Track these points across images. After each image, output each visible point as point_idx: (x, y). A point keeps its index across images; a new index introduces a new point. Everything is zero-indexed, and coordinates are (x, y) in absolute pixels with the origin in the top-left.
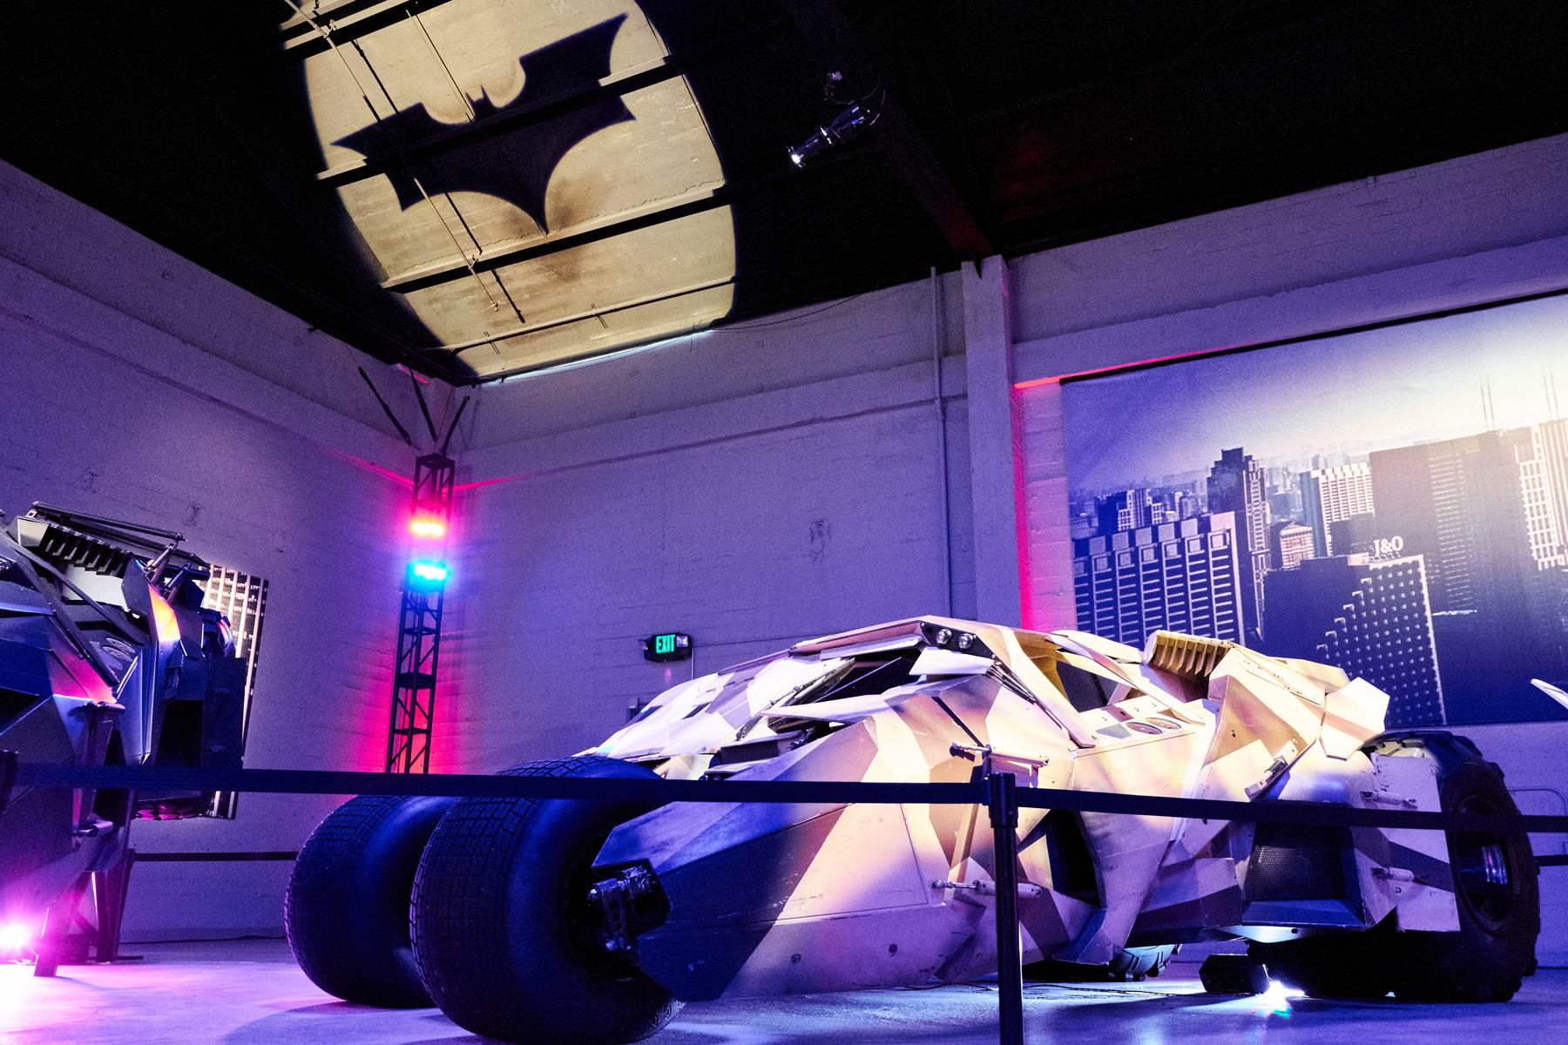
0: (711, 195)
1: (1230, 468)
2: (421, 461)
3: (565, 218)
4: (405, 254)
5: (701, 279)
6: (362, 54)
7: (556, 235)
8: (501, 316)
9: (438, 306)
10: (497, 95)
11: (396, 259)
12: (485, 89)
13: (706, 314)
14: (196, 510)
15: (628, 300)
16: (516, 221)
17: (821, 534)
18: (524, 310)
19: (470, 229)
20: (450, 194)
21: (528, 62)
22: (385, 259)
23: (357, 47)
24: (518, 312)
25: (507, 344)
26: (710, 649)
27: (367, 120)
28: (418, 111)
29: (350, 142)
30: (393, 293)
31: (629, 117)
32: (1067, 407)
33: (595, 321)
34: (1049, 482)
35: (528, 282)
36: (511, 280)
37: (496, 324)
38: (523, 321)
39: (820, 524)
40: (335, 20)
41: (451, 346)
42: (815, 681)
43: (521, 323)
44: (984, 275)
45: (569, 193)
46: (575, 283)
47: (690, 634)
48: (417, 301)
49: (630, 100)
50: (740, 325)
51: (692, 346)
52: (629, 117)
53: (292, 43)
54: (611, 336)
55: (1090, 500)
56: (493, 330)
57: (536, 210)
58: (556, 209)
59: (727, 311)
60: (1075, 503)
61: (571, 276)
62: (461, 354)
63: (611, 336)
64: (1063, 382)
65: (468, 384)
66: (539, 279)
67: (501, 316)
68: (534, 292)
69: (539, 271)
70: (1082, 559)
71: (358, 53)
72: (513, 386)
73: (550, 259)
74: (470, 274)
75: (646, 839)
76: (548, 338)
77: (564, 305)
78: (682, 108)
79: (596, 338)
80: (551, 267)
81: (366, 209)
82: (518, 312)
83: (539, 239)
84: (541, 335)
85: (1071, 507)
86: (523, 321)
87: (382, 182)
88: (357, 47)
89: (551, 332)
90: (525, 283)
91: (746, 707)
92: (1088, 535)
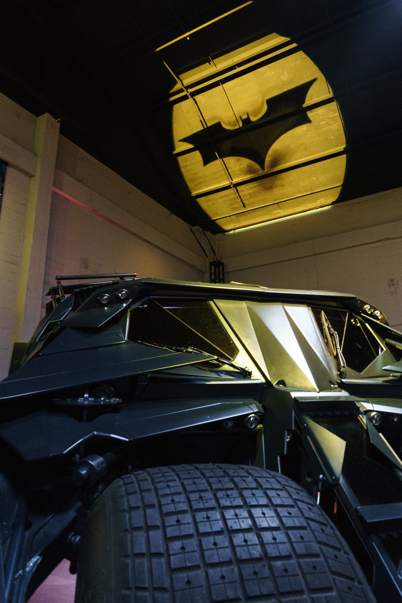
0: (343, 150)
1: (53, 288)
2: (211, 264)
8: (236, 206)
9: (210, 203)
12: (249, 114)
15: (288, 198)
17: (394, 285)
18: (246, 202)
19: (229, 171)
21: (269, 102)
22: (190, 185)
23: (194, 100)
24: (243, 204)
27: (199, 128)
28: (218, 125)
29: (185, 140)
31: (309, 121)
33: (276, 205)
36: (243, 191)
37: (233, 209)
38: (245, 207)
39: (392, 281)
40: (190, 89)
42: (322, 347)
48: (199, 200)
49: (310, 114)
51: (322, 213)
52: (309, 121)
57: (261, 163)
59: (336, 198)
61: (270, 188)
65: (220, 233)
66: (255, 190)
67: (236, 206)
74: (231, 188)
75: (235, 412)
79: (275, 212)
81: (186, 166)
82: (243, 204)
86: (245, 207)
88: (194, 100)
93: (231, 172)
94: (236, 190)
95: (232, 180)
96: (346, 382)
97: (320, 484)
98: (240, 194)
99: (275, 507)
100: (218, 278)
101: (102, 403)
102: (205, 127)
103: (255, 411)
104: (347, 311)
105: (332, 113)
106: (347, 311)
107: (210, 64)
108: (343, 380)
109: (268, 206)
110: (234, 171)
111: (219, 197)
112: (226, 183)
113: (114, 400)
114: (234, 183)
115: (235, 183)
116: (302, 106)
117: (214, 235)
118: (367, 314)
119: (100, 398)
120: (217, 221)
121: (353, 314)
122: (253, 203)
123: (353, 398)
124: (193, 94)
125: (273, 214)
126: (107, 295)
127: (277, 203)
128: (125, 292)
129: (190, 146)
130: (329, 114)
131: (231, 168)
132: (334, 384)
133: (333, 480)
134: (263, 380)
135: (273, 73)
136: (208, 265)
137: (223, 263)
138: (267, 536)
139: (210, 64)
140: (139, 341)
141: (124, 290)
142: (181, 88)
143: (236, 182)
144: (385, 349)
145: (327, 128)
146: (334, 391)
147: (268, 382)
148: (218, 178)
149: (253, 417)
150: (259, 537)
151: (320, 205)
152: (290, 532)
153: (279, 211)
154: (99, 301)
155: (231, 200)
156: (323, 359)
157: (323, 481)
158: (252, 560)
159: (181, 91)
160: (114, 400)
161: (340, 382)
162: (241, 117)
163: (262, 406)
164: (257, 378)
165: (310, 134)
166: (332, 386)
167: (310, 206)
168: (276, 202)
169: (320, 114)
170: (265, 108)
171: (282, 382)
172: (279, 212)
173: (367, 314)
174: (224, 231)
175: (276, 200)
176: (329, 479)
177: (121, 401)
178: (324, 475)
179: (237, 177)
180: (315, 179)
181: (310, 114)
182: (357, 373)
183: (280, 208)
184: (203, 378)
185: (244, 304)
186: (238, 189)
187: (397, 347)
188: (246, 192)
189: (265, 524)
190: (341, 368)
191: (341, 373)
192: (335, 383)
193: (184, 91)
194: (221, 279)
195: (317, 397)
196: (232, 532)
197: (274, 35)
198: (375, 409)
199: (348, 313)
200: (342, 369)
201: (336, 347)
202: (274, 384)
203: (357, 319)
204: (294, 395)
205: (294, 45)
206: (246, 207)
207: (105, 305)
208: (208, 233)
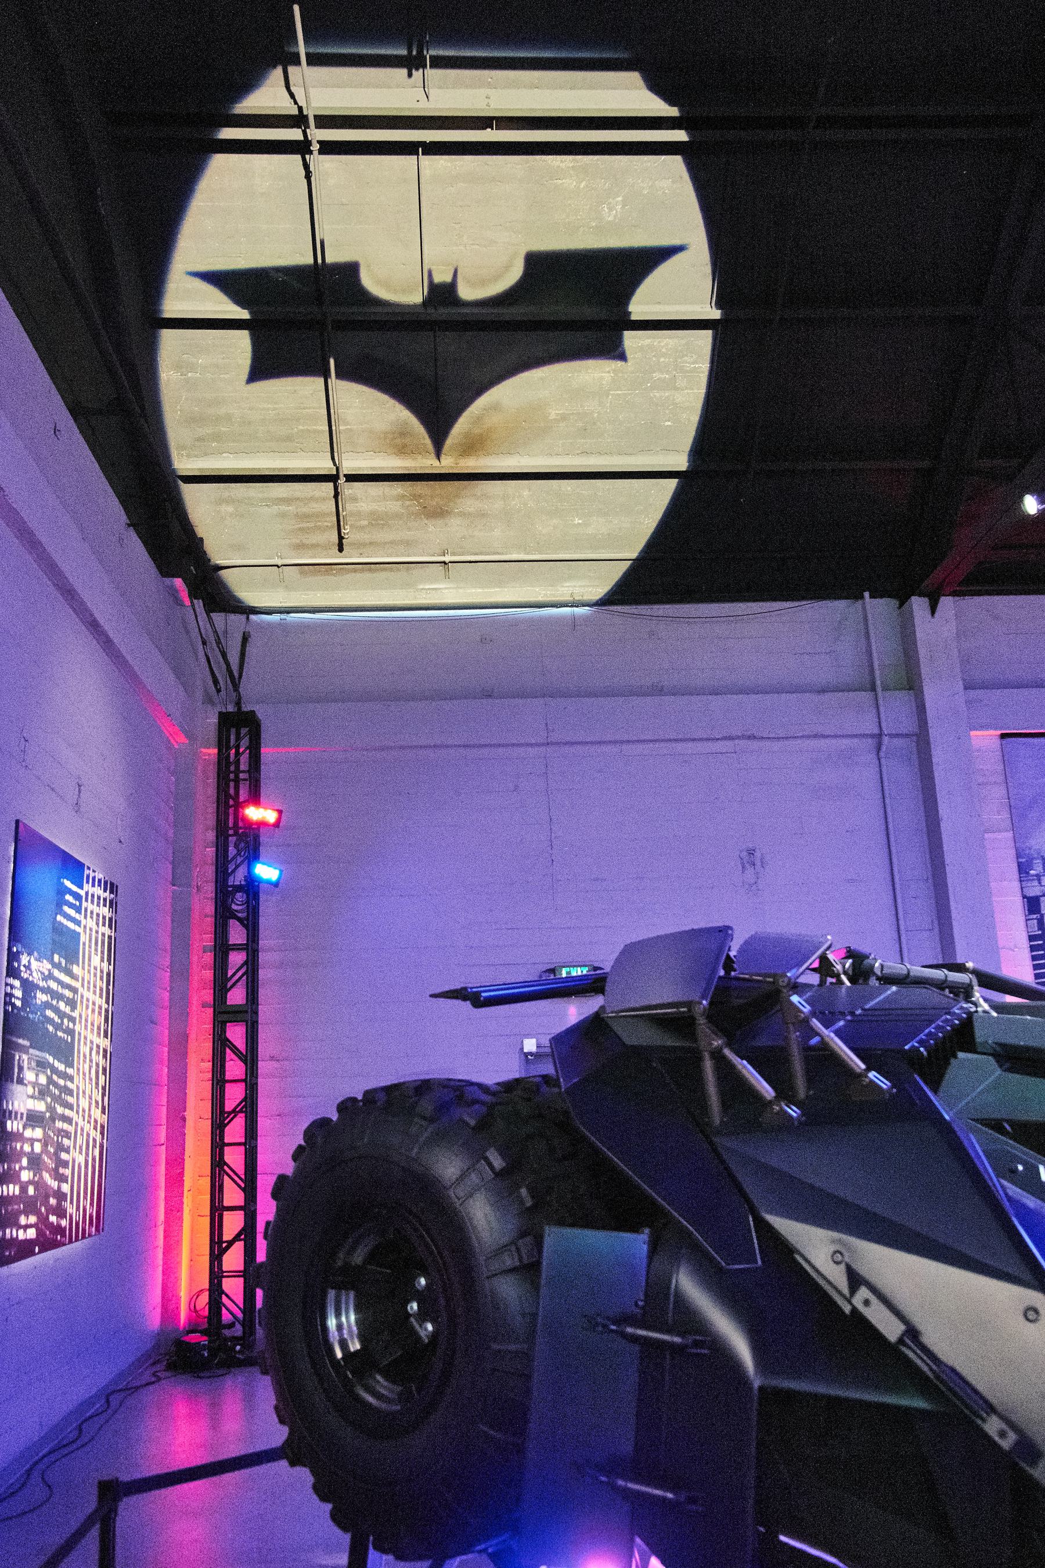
3: (472, 446)
4: (217, 437)
6: (308, 176)
7: (448, 463)
10: (472, 284)
13: (580, 586)
20: (672, 484)
23: (306, 166)
24: (341, 538)
25: (301, 573)
29: (220, 280)
30: (180, 482)
31: (622, 357)
32: (1005, 760)
33: (440, 567)
34: (996, 835)
36: (355, 499)
37: (300, 547)
38: (341, 549)
39: (751, 852)
44: (936, 615)
45: (494, 420)
46: (440, 522)
48: (189, 492)
49: (631, 339)
50: (626, 609)
52: (622, 357)
54: (446, 588)
55: (1038, 858)
58: (467, 435)
60: (1024, 860)
61: (439, 513)
62: (222, 573)
64: (1003, 736)
66: (395, 507)
68: (378, 520)
69: (402, 497)
70: (1035, 916)
71: (303, 173)
73: (420, 487)
77: (408, 543)
80: (416, 497)
82: (341, 538)
83: (428, 463)
84: (355, 571)
85: (1019, 865)
86: (341, 549)
88: (306, 166)
89: (370, 570)
90: (370, 508)
92: (1039, 894)
100: (233, 780)
105: (695, 357)
107: (410, 75)
109: (424, 565)
110: (351, 430)
120: (223, 573)
130: (686, 358)
135: (582, 185)
139: (410, 75)
140: (259, 1293)
145: (667, 394)
148: (289, 438)
153: (441, 586)
165: (617, 394)
168: (447, 559)
169: (664, 350)
170: (515, 273)
180: (579, 524)
181: (631, 339)
183: (447, 577)
188: (364, 506)
197: (634, 77)
205: (680, 136)
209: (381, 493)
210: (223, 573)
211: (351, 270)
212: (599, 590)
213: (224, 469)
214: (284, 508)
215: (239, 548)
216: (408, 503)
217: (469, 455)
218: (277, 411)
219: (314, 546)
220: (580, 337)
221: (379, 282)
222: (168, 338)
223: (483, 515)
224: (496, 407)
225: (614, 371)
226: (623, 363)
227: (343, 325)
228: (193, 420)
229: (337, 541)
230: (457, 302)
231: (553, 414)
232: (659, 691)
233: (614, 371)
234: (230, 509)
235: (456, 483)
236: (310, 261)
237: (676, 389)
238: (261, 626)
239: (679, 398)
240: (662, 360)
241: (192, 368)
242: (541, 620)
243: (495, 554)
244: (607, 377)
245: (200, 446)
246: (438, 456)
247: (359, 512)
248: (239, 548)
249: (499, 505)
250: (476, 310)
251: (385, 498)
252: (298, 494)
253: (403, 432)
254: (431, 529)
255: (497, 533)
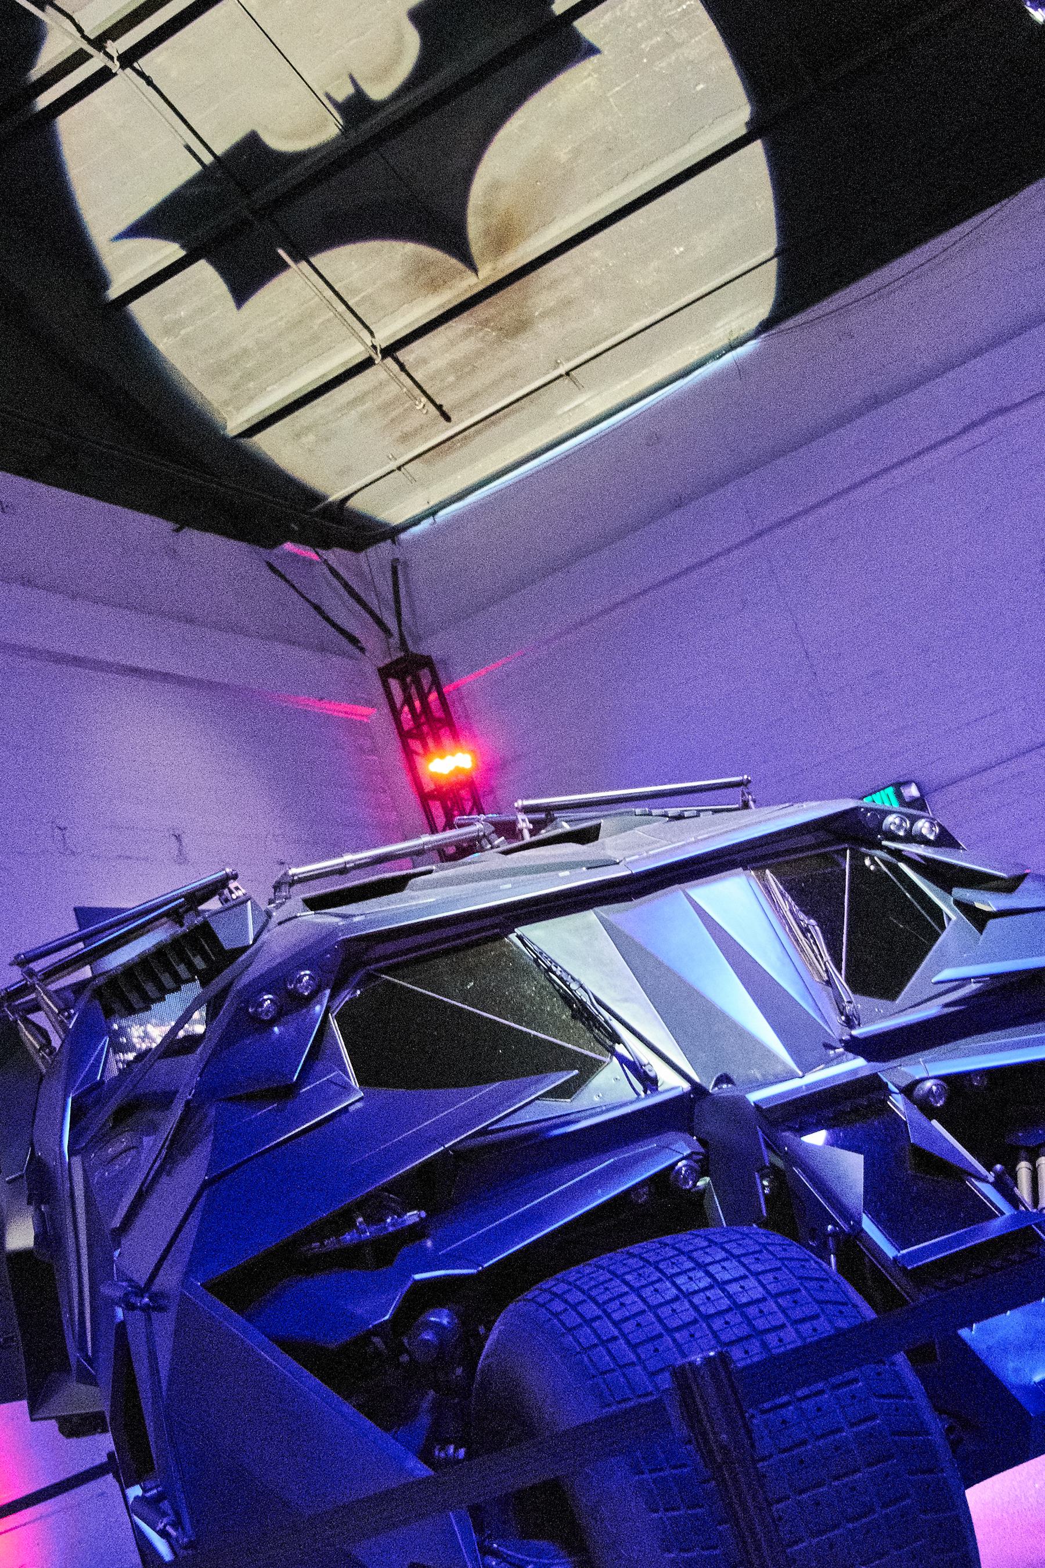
2: (385, 673)
4: (249, 376)
5: (722, 268)
6: (149, 82)
7: (489, 272)
11: (236, 387)
12: (355, 76)
14: (178, 838)
16: (420, 268)
19: (350, 303)
20: (313, 260)
23: (141, 74)
24: (439, 407)
26: (954, 791)
29: (143, 228)
30: (243, 441)
31: (592, 50)
33: (566, 381)
35: (448, 357)
36: (425, 361)
37: (405, 438)
38: (448, 419)
40: (114, 40)
41: (336, 496)
43: (446, 423)
45: (505, 200)
46: (528, 334)
47: (921, 778)
48: (266, 443)
52: (592, 50)
53: (44, 100)
54: (588, 399)
56: (402, 448)
58: (487, 232)
61: (521, 326)
63: (588, 399)
68: (464, 369)
72: (457, 523)
73: (482, 311)
76: (494, 432)
77: (513, 374)
78: (673, 13)
79: (566, 408)
80: (485, 323)
82: (439, 407)
83: (468, 284)
86: (448, 419)
87: (203, 271)
88: (141, 74)
91: (181, 1000)
93: (357, 304)
94: (395, 368)
95: (372, 333)
96: (860, 1034)
97: (831, 1242)
98: (418, 377)
99: (737, 1258)
101: (391, 1229)
102: (208, 159)
103: (685, 1154)
104: (846, 845)
106: (846, 845)
108: (854, 1032)
111: (339, 410)
112: (354, 352)
113: (412, 1216)
114: (384, 346)
115: (388, 343)
116: (552, 12)
117: (363, 554)
118: (894, 838)
119: (384, 1221)
120: (351, 503)
121: (863, 850)
122: (476, 395)
123: (877, 1067)
124: (128, 59)
125: (561, 415)
126: (266, 997)
127: (568, 374)
128: (307, 977)
129: (171, 251)
131: (355, 291)
132: (834, 1048)
133: (851, 1227)
134: (686, 1086)
136: (377, 683)
137: (429, 658)
138: (734, 1288)
141: (302, 973)
142: (74, 50)
143: (388, 338)
144: (954, 918)
146: (838, 1063)
147: (698, 1089)
148: (315, 338)
149: (684, 1166)
150: (723, 1290)
151: (726, 342)
152: (760, 1277)
154: (255, 1018)
155: (385, 408)
156: (803, 997)
157: (834, 1234)
158: (720, 1313)
159: (79, 58)
160: (412, 1216)
161: (848, 1037)
162: (329, 97)
163: (698, 1140)
164: (671, 1084)
166: (832, 1052)
167: (694, 351)
168: (562, 370)
170: (412, 41)
171: (724, 1079)
172: (582, 404)
173: (894, 838)
174: (392, 533)
175: (557, 365)
176: (845, 1228)
177: (423, 1214)
178: (835, 1224)
179: (386, 319)
182: (887, 1003)
183: (580, 387)
184: (562, 1120)
185: (590, 916)
186: (401, 359)
187: (978, 905)
188: (439, 363)
189: (727, 1277)
190: (844, 1008)
191: (847, 1016)
192: (838, 1044)
193: (90, 56)
194: (439, 720)
195: (801, 1087)
196: (689, 1295)
198: (931, 1075)
199: (848, 851)
200: (848, 1008)
201: (822, 957)
202: (710, 1088)
203: (876, 858)
204: (754, 1097)
206: (452, 416)
207: (273, 1022)
208: (335, 556)
209: (445, 340)
210: (351, 503)
211: (252, 143)
212: (763, 311)
213: (309, 384)
214: (360, 409)
215: (345, 472)
216: (481, 334)
217: (507, 249)
218: (285, 320)
219: (416, 432)
220: (529, 61)
221: (287, 137)
222: (138, 308)
223: (567, 303)
224: (495, 186)
225: (594, 70)
226: (598, 56)
227: (280, 202)
228: (220, 371)
229: (437, 413)
230: (373, 107)
231: (563, 154)
232: (875, 402)
233: (594, 70)
234: (311, 437)
235: (516, 286)
236: (198, 168)
237: (679, 45)
238: (416, 542)
239: (689, 53)
240: (639, 25)
241: (180, 323)
242: (706, 384)
243: (606, 338)
244: (591, 81)
245: (240, 397)
246: (475, 270)
247: (438, 371)
248: (345, 472)
249: (577, 282)
250: (400, 103)
251: (452, 343)
252: (365, 388)
253: (420, 268)
254: (524, 347)
255: (597, 311)
